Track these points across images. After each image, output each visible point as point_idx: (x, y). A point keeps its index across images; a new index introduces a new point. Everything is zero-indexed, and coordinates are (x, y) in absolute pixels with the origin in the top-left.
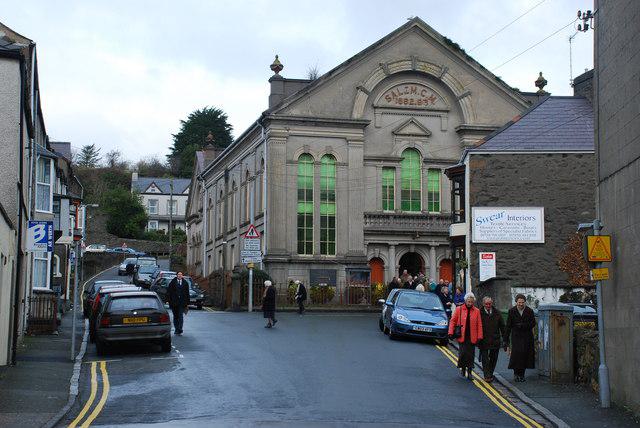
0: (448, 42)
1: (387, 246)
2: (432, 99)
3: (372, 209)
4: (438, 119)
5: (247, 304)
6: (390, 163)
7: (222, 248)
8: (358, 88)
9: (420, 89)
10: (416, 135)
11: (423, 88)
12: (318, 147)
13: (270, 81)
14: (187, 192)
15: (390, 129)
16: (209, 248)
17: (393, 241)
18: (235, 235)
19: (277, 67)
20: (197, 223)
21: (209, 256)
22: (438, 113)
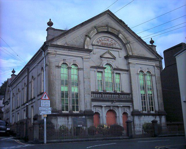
0: (121, 21)
1: (101, 107)
2: (115, 44)
3: (93, 90)
4: (117, 53)
5: (43, 139)
6: (100, 69)
7: (25, 108)
8: (86, 36)
9: (110, 39)
10: (109, 58)
12: (70, 61)
13: (47, 30)
14: (3, 99)
15: (99, 55)
16: (13, 112)
17: (104, 104)
18: (19, 109)
19: (50, 24)
20: (7, 104)
21: (13, 116)
22: (118, 50)
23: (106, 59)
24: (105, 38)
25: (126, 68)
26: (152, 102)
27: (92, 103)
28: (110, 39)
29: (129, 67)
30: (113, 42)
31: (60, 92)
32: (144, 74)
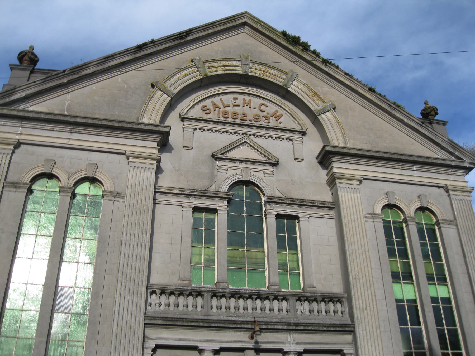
2: (278, 117)
9: (256, 102)
11: (261, 101)
23: (237, 164)
24: (236, 96)
25: (327, 197)
26: (453, 334)
27: (150, 332)
28: (254, 99)
29: (335, 195)
30: (267, 110)
31: (429, 300)
32: (405, 218)
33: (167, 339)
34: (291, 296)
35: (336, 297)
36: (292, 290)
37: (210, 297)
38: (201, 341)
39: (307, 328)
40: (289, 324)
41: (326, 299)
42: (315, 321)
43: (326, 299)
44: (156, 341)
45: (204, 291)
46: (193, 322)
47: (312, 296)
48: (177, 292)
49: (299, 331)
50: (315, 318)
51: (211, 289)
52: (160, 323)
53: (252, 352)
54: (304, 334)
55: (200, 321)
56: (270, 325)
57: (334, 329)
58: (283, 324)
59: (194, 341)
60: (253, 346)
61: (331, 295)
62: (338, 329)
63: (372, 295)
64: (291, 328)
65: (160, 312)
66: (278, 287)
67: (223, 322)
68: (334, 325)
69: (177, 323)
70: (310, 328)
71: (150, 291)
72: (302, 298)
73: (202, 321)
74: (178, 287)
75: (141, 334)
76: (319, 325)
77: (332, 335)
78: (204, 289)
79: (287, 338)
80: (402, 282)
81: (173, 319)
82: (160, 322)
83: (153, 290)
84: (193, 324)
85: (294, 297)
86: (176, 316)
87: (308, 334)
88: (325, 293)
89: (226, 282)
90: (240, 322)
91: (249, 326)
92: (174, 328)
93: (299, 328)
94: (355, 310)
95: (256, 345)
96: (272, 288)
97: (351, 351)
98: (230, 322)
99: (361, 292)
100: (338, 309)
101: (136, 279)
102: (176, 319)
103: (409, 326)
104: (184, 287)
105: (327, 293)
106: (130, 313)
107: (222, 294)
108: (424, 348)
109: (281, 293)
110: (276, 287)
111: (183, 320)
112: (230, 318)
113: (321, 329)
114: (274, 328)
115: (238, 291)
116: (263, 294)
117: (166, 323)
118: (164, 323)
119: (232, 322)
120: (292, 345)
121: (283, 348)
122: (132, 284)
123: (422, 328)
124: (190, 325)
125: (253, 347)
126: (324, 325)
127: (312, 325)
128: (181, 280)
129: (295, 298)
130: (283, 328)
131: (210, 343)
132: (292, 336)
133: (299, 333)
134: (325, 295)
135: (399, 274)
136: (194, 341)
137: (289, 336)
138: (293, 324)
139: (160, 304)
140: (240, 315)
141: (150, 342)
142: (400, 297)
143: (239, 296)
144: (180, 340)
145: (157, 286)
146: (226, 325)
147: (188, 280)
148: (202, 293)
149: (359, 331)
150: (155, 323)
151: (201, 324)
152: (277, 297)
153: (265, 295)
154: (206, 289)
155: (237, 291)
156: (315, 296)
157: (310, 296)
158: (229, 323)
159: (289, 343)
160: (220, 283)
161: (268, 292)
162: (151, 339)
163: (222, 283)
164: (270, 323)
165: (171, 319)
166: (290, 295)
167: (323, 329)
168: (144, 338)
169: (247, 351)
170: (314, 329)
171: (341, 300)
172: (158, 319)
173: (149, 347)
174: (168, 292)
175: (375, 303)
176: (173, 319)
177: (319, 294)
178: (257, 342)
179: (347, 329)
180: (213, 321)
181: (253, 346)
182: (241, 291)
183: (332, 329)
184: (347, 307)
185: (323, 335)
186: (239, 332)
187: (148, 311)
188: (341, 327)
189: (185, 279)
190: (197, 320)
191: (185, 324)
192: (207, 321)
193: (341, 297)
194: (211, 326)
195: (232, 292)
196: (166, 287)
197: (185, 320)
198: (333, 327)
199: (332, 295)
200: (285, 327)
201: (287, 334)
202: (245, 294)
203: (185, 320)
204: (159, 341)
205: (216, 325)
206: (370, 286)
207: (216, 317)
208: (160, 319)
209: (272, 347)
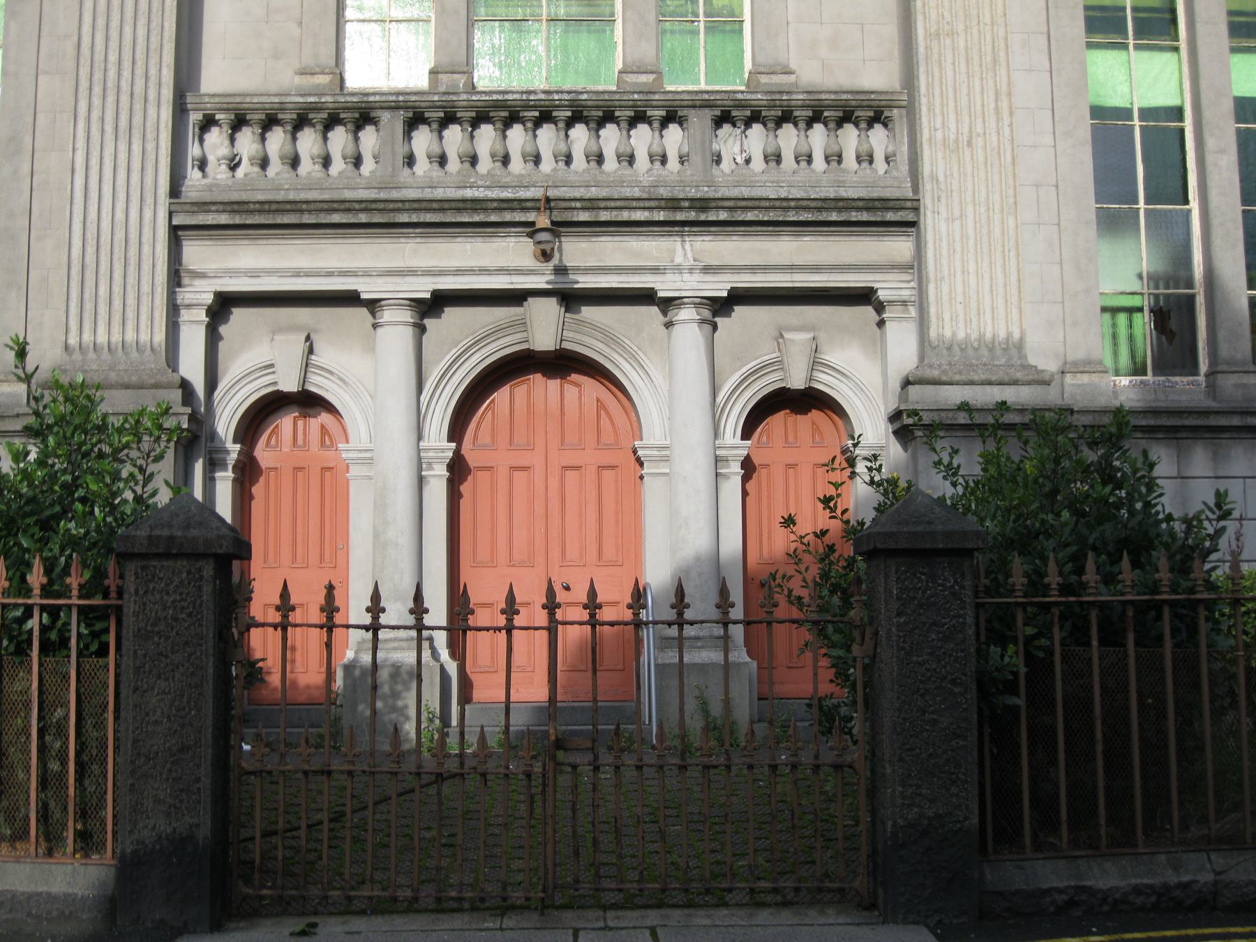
27: (196, 253)
31: (1228, 106)
33: (254, 274)
34: (694, 107)
35: (865, 103)
36: (709, 88)
37: (399, 128)
38: (367, 274)
39: (740, 216)
40: (673, 204)
41: (826, 114)
42: (777, 192)
43: (826, 114)
44: (219, 281)
45: (377, 104)
46: (336, 210)
47: (772, 105)
48: (289, 116)
49: (713, 229)
50: (778, 182)
51: (401, 98)
52: (223, 222)
53: (551, 305)
54: (735, 238)
55: (357, 206)
56: (606, 208)
57: (843, 217)
58: (653, 204)
59: (344, 273)
60: (548, 283)
61: (844, 97)
62: (855, 216)
63: (997, 93)
64: (680, 216)
65: (230, 187)
66: (651, 77)
67: (435, 205)
68: (841, 204)
69: (280, 219)
70: (750, 216)
71: (195, 117)
72: (734, 113)
73: (363, 205)
74: (288, 99)
75: (161, 260)
76: (785, 204)
77: (837, 238)
78: (377, 98)
79: (674, 251)
80: (1131, 42)
81: (266, 207)
82: (223, 219)
83: (204, 115)
84: (336, 218)
85: (707, 111)
86: (280, 196)
87: (746, 238)
88: (821, 92)
89: (460, 70)
90: (495, 204)
91: (528, 214)
92: (276, 237)
93: (712, 216)
94: (926, 147)
95: (560, 279)
96: (628, 80)
97: (905, 294)
98: (460, 205)
99: (955, 82)
100: (871, 147)
101: (139, 83)
102: (274, 207)
103: (1141, 204)
104: (310, 95)
105: (830, 92)
106: (121, 196)
107: (445, 112)
108: (1190, 283)
109: (657, 97)
110: (644, 78)
111: (299, 206)
112: (469, 193)
113: (792, 216)
114: (619, 219)
115: (500, 97)
116: (589, 103)
117: (242, 222)
118: (238, 220)
119: (469, 205)
120: (687, 277)
121: (657, 286)
122: (125, 99)
123: (1189, 211)
124: (323, 221)
125: (550, 287)
126: (801, 203)
127: (757, 203)
128: (303, 73)
129: (708, 115)
130: (650, 219)
131: (398, 279)
132: (691, 245)
133: (715, 234)
134: (823, 97)
135: (1121, 14)
136: (344, 273)
137: (679, 245)
138: (687, 204)
139: (232, 160)
140: (504, 180)
141: (200, 284)
142: (1116, 98)
143: (505, 114)
144: (297, 274)
145: (217, 100)
146: (450, 217)
147: (327, 70)
148: (373, 114)
149: (934, 222)
150: (209, 223)
151: (363, 218)
152: (645, 112)
153: (598, 107)
154: (384, 98)
155: (495, 97)
156: (785, 103)
157: (765, 102)
158: (458, 210)
159: (678, 269)
160: (441, 76)
161: (607, 97)
162: (203, 276)
163: (446, 73)
164: (602, 204)
165: (257, 206)
166: (690, 103)
167: (801, 218)
168: (176, 276)
169: (530, 300)
170: (766, 219)
171: (886, 114)
172: (214, 208)
173: (195, 302)
174: (256, 117)
175: (1006, 121)
176: (266, 207)
177: (801, 97)
178: (561, 270)
179: (890, 216)
180: (400, 205)
181: (548, 283)
182: (510, 97)
183: (834, 217)
184: (906, 140)
185: (806, 238)
186: (500, 240)
187: (188, 186)
188: (868, 209)
189: (317, 70)
190: (347, 205)
191: (307, 219)
192: (381, 206)
193: (884, 103)
194: (397, 220)
195: (479, 104)
196: (248, 100)
197: (304, 206)
198: (840, 210)
199: (850, 97)
200: (661, 216)
201: (672, 238)
202: (527, 106)
203: (304, 206)
204: (226, 281)
205: (415, 218)
206: (995, 61)
207: (420, 190)
208: (221, 208)
209: (615, 285)
